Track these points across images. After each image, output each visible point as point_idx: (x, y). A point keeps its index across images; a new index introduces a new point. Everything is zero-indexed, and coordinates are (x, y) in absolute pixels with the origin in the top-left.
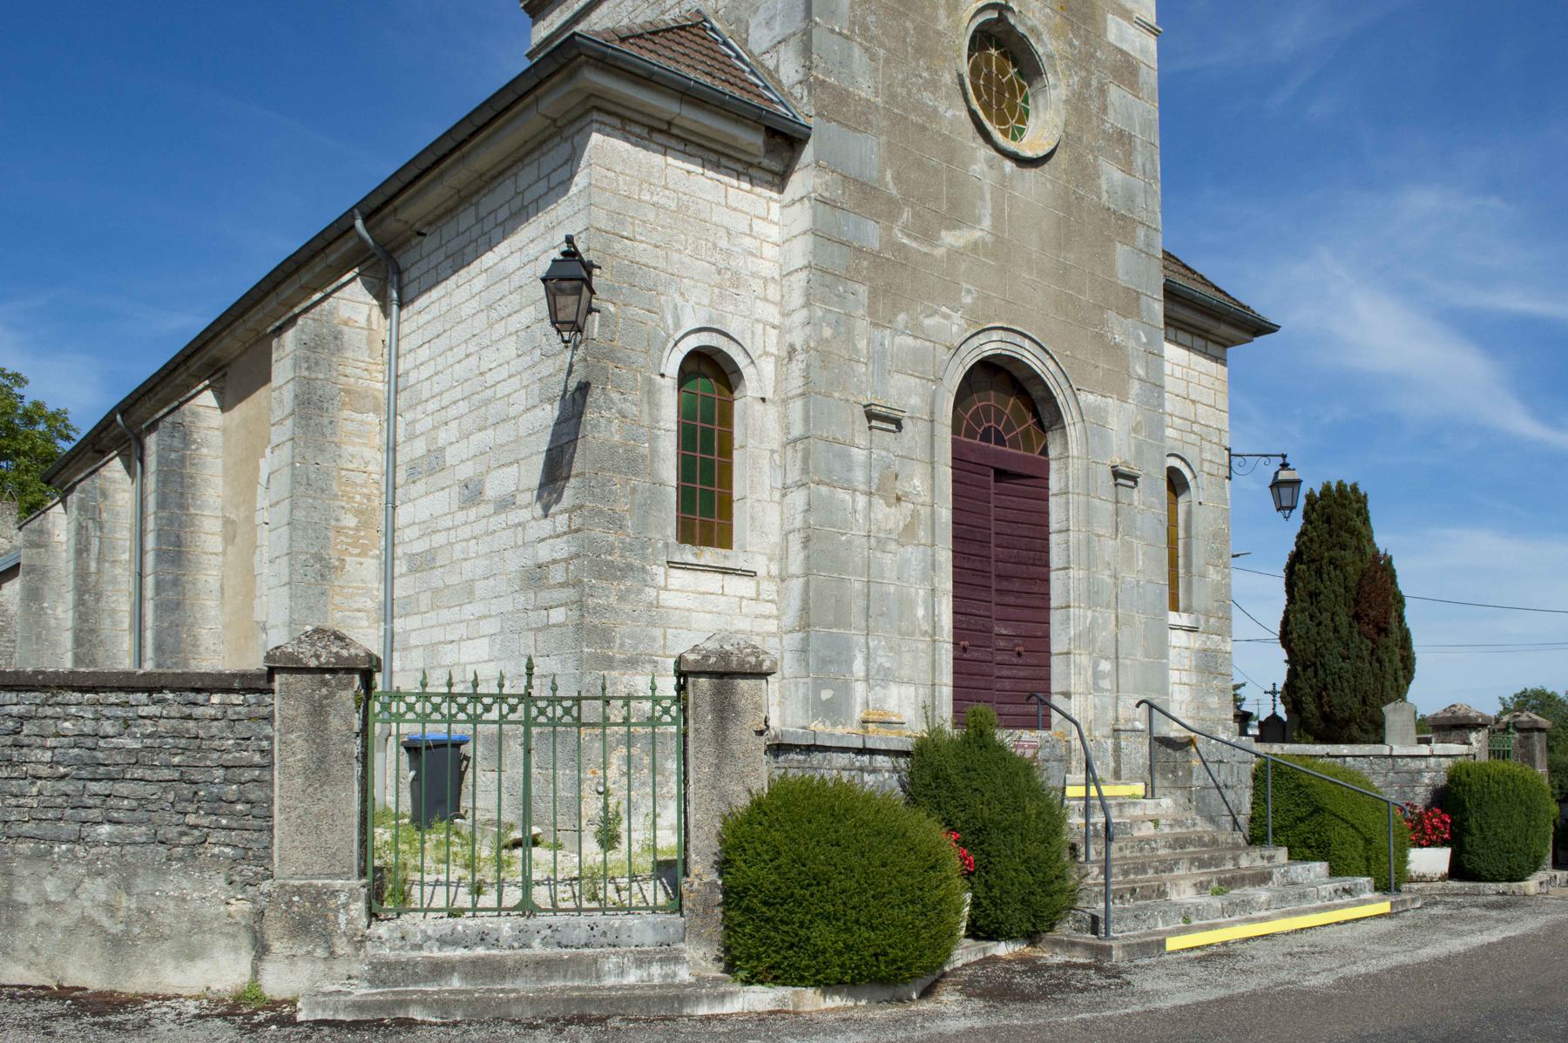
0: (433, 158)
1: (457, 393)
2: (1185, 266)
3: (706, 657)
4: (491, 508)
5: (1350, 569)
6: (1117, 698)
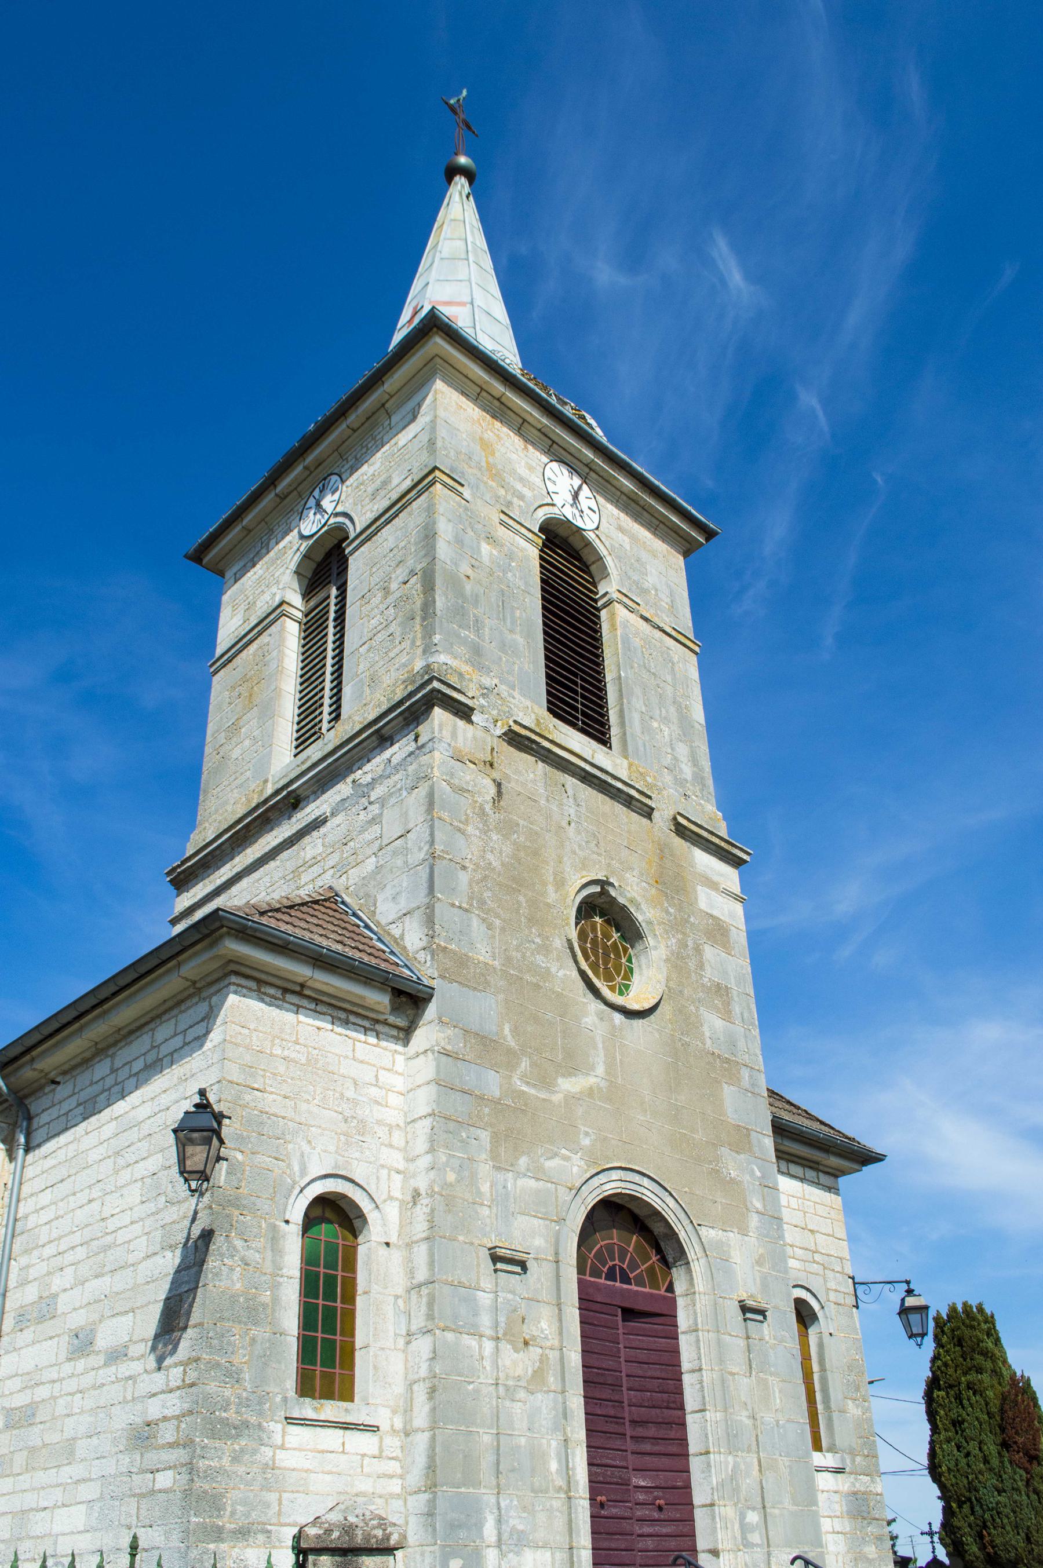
0: (75, 1014)
1: (77, 1238)
2: (789, 1102)
3: (329, 1531)
4: (101, 1359)
5: (990, 1393)
6: (769, 1554)
